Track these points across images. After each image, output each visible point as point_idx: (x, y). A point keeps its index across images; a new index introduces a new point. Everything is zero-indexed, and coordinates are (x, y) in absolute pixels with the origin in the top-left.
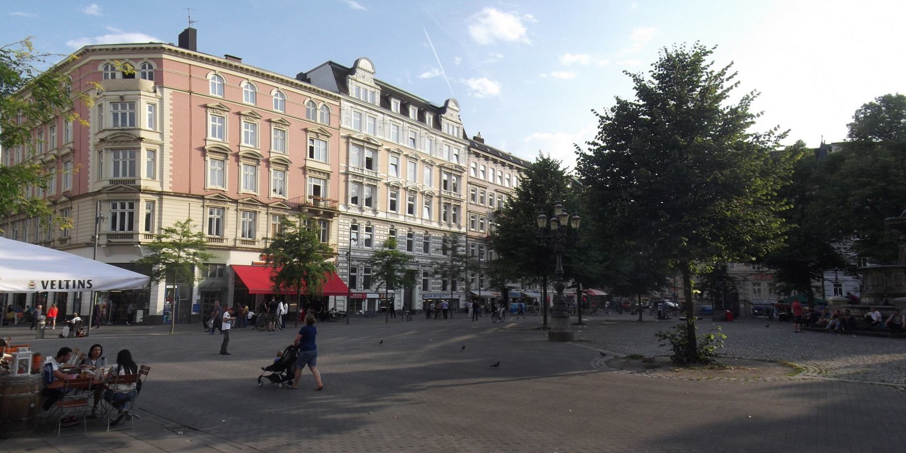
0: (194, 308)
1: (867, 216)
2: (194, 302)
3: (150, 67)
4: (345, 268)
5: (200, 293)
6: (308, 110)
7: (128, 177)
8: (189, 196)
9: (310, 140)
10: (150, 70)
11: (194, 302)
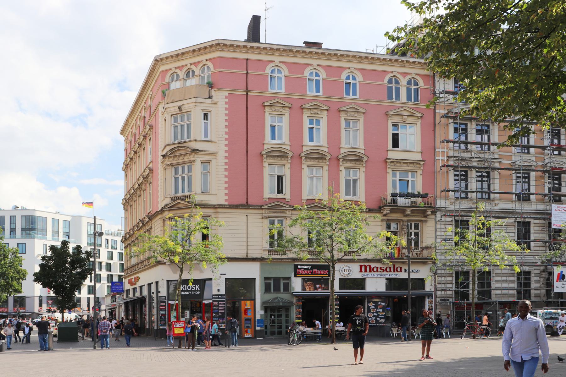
0: (257, 323)
1: (517, 10)
2: (258, 317)
3: (416, 84)
4: (449, 282)
5: (264, 308)
6: (390, 89)
7: (186, 193)
8: (246, 206)
9: (393, 125)
10: (416, 87)
11: (258, 317)
